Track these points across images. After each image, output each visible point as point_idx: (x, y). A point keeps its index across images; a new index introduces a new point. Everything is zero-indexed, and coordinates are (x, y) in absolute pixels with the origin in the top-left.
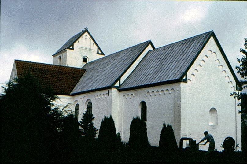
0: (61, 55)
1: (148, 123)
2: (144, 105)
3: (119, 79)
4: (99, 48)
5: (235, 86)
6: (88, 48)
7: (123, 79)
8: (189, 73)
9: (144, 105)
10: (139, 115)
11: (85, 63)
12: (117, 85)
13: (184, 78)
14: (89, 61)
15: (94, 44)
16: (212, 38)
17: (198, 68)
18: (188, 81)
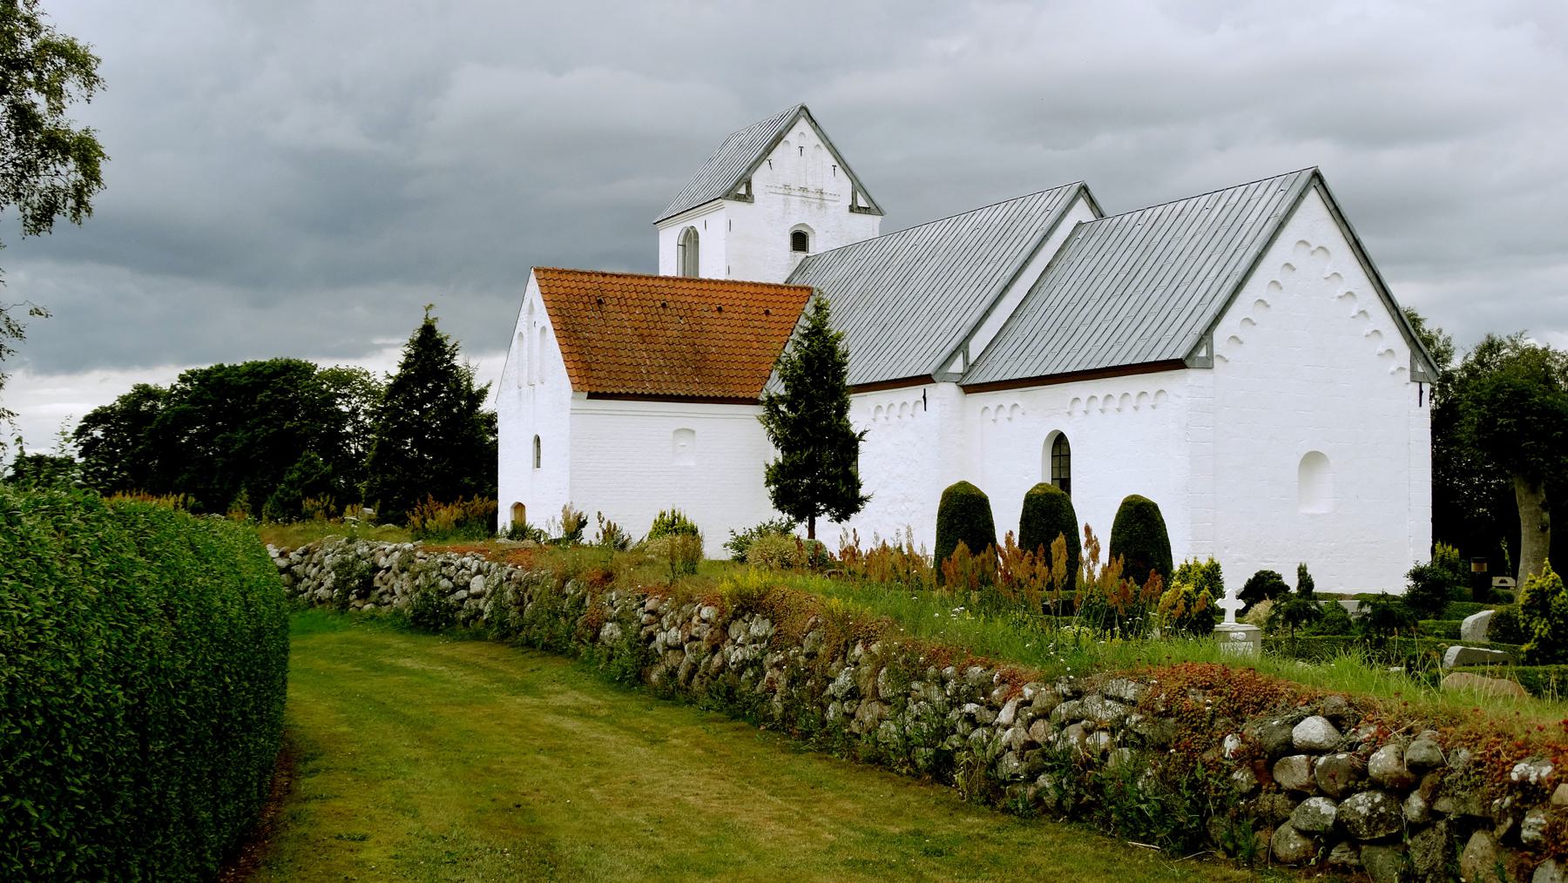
0: (698, 224)
1: (1078, 499)
2: (1060, 445)
3: (963, 347)
4: (858, 187)
5: (1408, 366)
6: (811, 189)
7: (976, 346)
8: (1219, 334)
9: (1060, 445)
10: (760, 410)
11: (801, 255)
12: (957, 366)
13: (1203, 353)
14: (816, 246)
15: (838, 168)
16: (1313, 197)
17: (1301, 259)
18: (1217, 362)
